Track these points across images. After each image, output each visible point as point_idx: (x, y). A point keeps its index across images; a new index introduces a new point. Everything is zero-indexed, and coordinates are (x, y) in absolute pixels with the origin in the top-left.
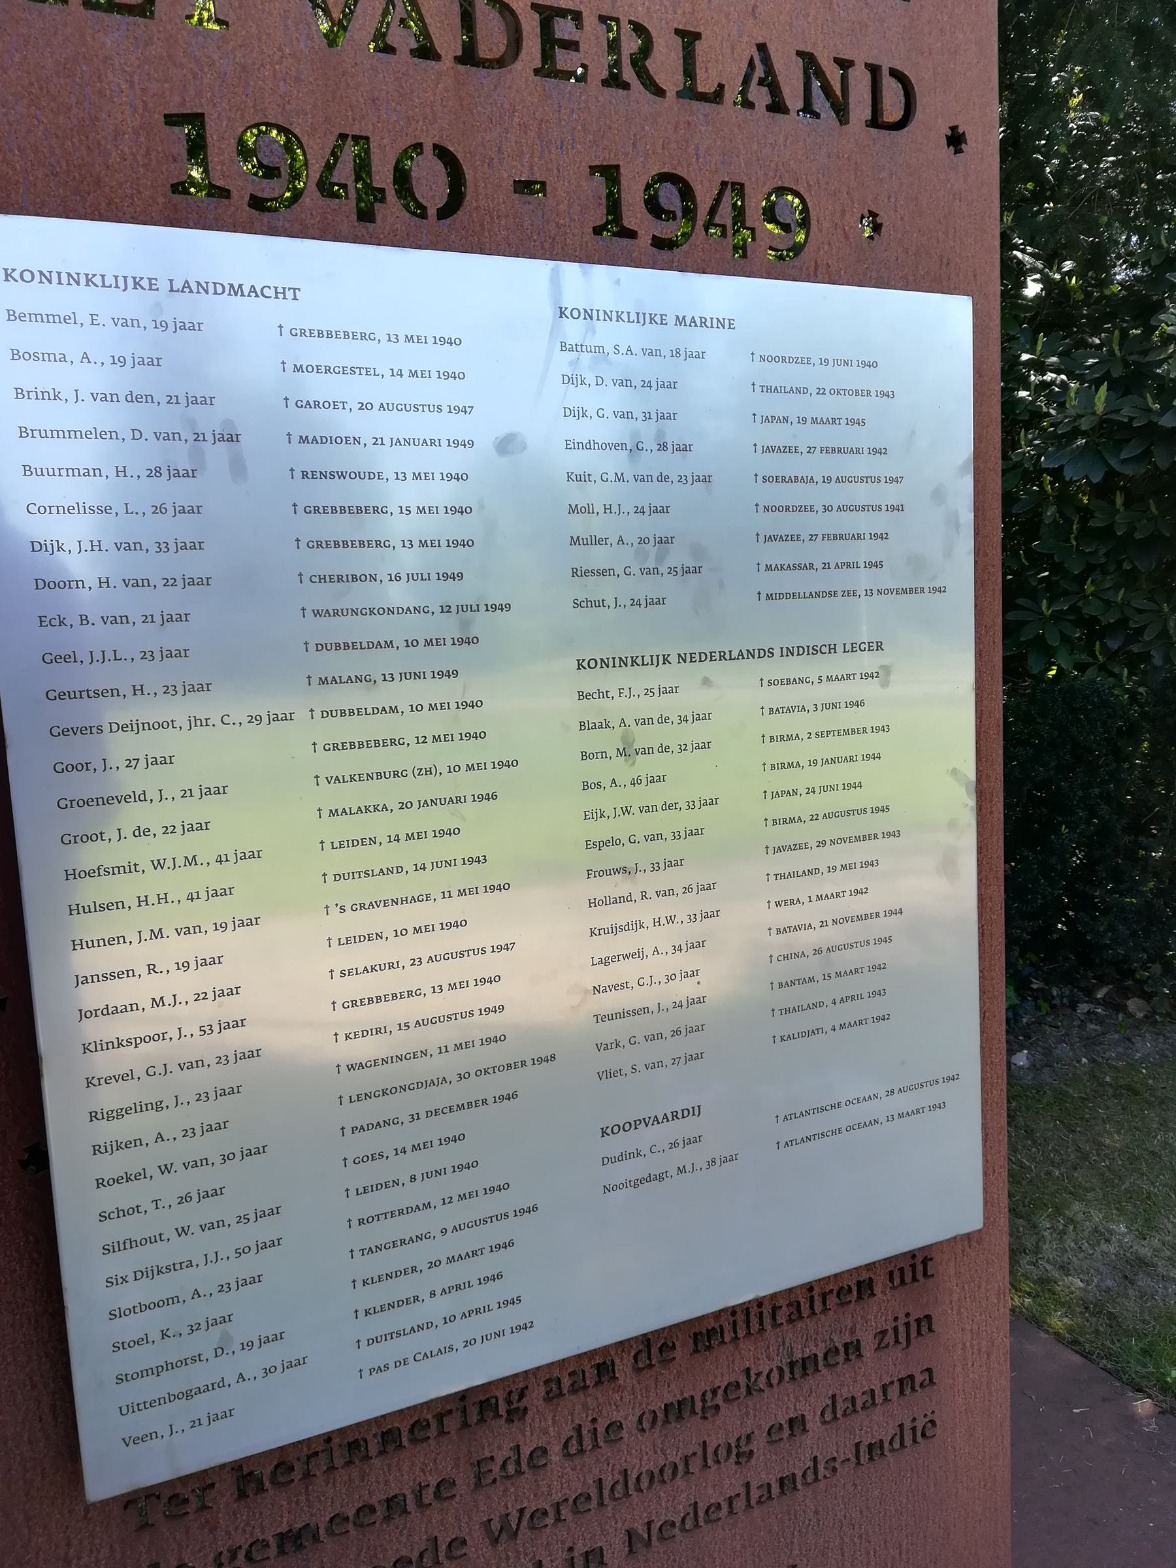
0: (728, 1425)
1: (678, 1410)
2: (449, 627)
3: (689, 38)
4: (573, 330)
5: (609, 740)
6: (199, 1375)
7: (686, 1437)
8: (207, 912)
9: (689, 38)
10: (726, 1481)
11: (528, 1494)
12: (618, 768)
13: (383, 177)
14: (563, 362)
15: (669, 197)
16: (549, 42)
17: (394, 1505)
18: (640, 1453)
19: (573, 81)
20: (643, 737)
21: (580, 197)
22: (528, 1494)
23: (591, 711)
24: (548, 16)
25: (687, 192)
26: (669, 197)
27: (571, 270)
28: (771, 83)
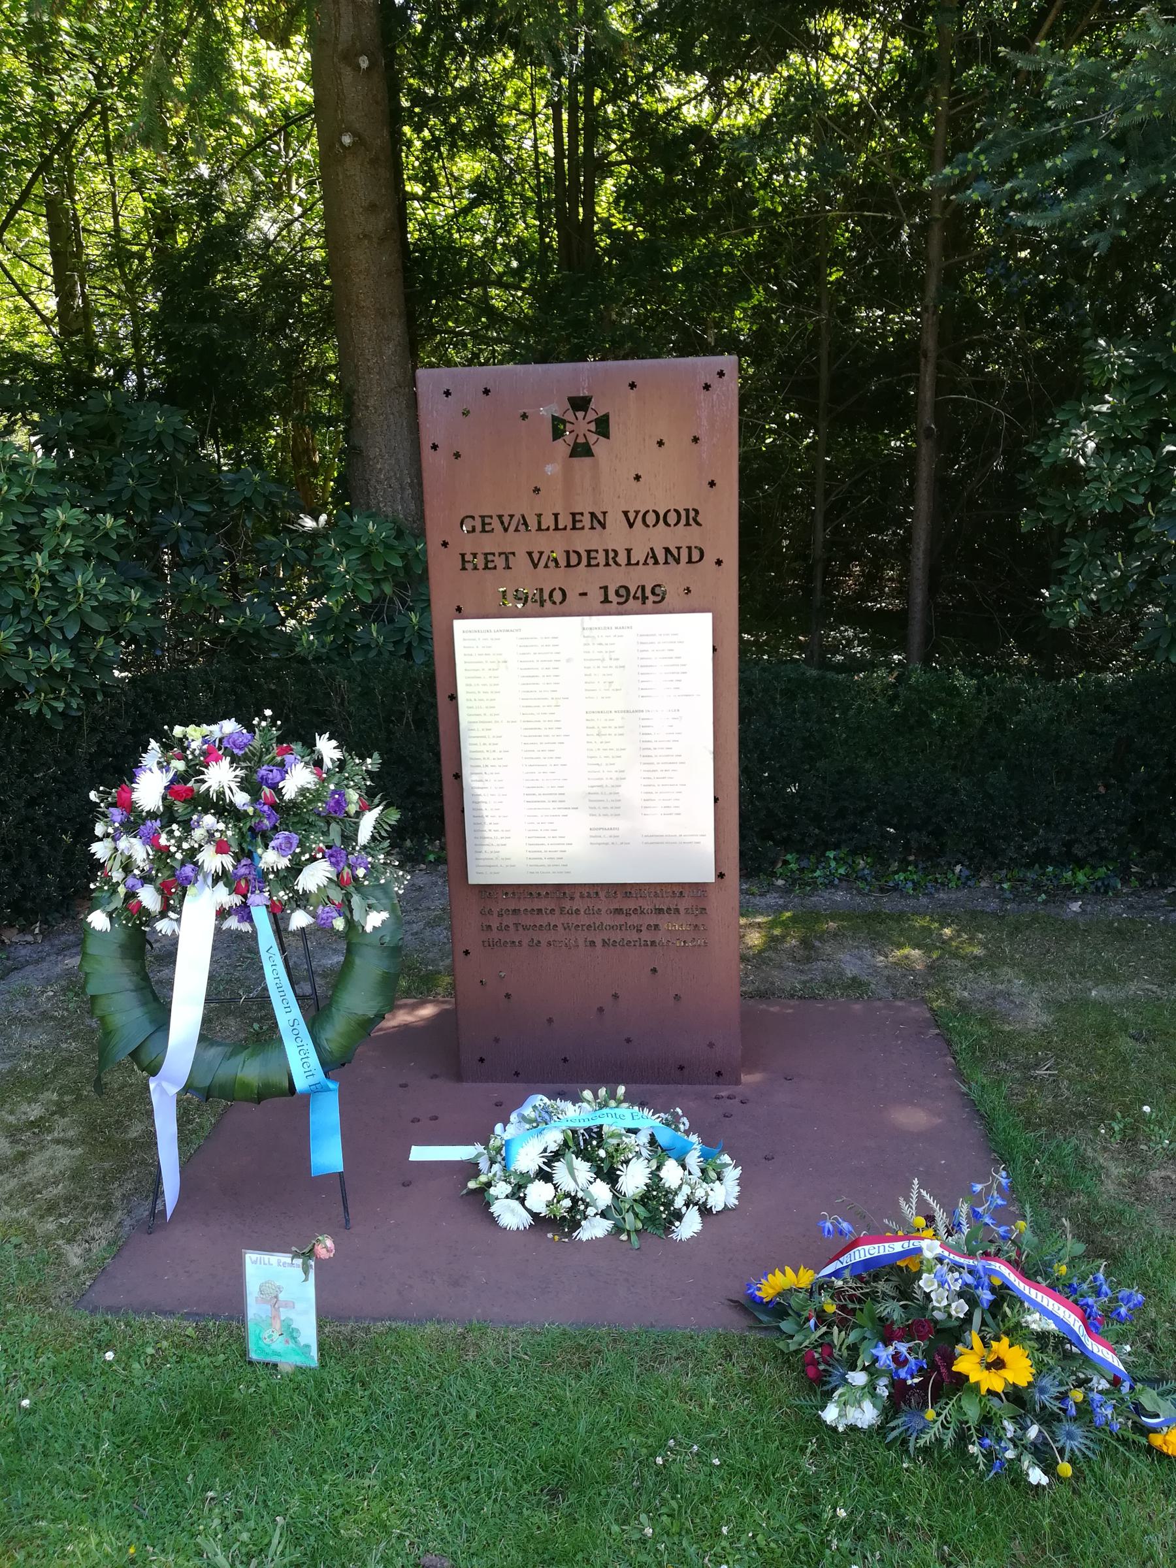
0: (634, 920)
1: (618, 911)
2: (554, 703)
3: (629, 551)
4: (587, 633)
5: (595, 731)
6: (543, 920)
7: (621, 920)
8: (497, 763)
9: (629, 551)
10: (633, 936)
11: (573, 920)
12: (598, 739)
13: (546, 596)
14: (584, 640)
15: (622, 592)
16: (589, 558)
17: (540, 911)
18: (608, 920)
19: (1004, 204)
20: (603, 731)
21: (596, 595)
22: (573, 920)
23: (590, 724)
24: (589, 552)
25: (627, 589)
26: (622, 592)
27: (586, 618)
28: (654, 557)
